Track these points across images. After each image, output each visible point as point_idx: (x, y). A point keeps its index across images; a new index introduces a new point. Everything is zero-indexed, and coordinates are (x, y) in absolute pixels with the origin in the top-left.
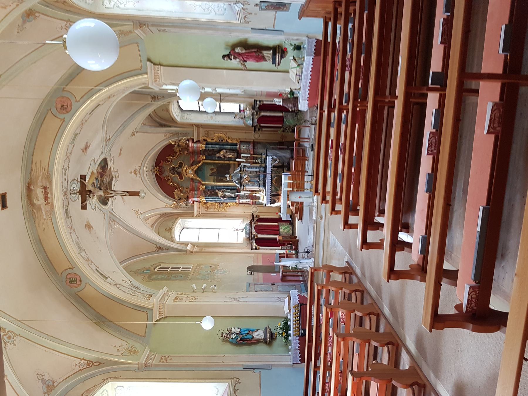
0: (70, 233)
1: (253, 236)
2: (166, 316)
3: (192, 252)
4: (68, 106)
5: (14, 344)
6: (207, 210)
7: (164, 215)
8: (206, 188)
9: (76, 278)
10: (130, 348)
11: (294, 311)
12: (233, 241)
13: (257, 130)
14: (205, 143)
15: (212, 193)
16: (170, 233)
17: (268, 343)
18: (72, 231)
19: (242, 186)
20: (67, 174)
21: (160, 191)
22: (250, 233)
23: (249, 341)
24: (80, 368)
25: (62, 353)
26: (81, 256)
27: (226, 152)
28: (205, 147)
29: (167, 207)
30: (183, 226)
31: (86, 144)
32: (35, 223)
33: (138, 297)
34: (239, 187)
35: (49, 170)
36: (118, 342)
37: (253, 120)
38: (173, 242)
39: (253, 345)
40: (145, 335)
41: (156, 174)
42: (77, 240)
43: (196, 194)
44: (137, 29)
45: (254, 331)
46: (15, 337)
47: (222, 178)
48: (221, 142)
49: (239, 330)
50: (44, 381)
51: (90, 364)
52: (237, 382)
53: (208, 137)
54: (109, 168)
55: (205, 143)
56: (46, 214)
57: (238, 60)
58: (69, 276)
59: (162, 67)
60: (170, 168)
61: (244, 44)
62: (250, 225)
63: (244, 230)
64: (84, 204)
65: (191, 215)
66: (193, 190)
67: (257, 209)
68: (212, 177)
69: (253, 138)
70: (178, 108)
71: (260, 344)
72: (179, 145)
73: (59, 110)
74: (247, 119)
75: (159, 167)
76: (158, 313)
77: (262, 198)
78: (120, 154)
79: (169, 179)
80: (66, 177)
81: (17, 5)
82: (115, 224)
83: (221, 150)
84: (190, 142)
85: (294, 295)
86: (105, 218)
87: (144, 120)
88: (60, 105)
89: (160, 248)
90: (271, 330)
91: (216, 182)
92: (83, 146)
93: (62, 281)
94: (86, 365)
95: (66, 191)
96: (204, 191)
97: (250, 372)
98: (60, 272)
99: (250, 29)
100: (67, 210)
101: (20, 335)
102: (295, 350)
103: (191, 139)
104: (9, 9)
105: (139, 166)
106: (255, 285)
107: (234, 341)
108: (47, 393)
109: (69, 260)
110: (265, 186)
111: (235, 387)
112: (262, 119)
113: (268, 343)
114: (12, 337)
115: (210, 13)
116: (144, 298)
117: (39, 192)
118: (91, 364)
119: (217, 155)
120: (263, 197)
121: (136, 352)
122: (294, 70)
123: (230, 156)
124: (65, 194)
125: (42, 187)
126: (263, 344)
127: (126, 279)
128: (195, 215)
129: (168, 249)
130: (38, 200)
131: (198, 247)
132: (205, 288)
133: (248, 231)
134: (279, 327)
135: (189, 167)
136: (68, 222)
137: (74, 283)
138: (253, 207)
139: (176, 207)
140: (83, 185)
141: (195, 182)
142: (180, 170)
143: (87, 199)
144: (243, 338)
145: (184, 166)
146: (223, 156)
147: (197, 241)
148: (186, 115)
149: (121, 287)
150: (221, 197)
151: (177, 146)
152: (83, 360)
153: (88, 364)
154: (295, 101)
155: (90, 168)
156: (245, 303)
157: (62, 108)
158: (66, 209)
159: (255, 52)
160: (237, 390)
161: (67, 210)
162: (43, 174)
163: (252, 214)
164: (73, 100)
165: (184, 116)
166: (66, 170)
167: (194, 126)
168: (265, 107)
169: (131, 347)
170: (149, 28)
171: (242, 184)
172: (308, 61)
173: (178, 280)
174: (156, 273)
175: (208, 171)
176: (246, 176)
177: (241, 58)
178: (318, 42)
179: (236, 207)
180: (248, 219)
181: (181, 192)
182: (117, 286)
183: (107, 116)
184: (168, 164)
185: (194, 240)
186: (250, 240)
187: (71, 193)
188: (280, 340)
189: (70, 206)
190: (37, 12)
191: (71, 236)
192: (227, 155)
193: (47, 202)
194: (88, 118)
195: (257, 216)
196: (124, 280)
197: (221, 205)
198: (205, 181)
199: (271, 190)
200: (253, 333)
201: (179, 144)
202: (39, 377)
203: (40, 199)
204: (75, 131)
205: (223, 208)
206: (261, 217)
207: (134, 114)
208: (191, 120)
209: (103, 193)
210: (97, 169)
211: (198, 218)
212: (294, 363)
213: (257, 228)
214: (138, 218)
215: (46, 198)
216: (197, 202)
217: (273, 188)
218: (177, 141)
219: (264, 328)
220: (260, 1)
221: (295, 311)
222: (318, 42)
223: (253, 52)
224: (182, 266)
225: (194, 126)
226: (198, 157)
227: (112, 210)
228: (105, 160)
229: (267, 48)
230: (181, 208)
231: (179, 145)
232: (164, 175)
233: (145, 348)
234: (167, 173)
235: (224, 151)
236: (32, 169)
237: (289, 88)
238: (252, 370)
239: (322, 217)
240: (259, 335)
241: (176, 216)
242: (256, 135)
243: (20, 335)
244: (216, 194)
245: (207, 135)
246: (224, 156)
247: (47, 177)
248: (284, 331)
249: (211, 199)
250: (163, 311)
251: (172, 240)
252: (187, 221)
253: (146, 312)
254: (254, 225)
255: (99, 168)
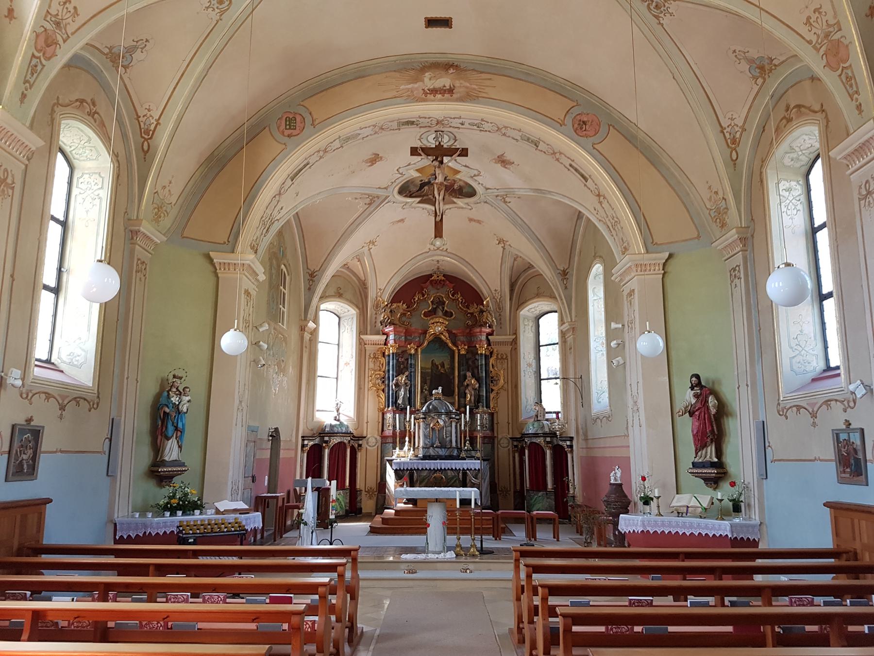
0: (375, 126)
1: (326, 439)
2: (219, 275)
3: (303, 329)
4: (584, 132)
5: (207, 8)
6: (372, 356)
7: (363, 286)
8: (411, 355)
9: (295, 129)
10: (164, 208)
11: (229, 521)
12: (319, 404)
13: (515, 443)
14: (488, 353)
15: (403, 363)
16: (334, 294)
17: (155, 469)
18: (377, 129)
19: (423, 416)
20: (472, 127)
21: (405, 280)
22: (332, 434)
23: (162, 430)
24: (142, 116)
25: (175, 88)
26: (334, 141)
27: (476, 389)
28: (481, 354)
29: (378, 291)
30: (343, 317)
31: (511, 161)
32: (391, 71)
33: (257, 228)
34: (421, 411)
35: (480, 99)
36: (177, 189)
37: (536, 435)
38: (321, 298)
39: (150, 439)
40: (184, 237)
41: (431, 276)
42: (361, 136)
43: (400, 338)
44: (737, 233)
45: (179, 440)
46: (219, 11)
47: (428, 382)
48: (491, 379)
49: (185, 410)
50: (131, 50)
51: (147, 135)
52: (91, 403)
53: (497, 358)
54: (455, 200)
55: (488, 353)
56: (408, 90)
57: (693, 401)
58: (298, 118)
59: (661, 276)
60: (443, 297)
61: (723, 411)
62: (348, 433)
63: (338, 423)
64: (420, 152)
65: (362, 330)
66: (408, 333)
67: (373, 446)
68: (429, 365)
69: (500, 437)
70: (543, 311)
71: (152, 454)
72: (482, 311)
73: (578, 118)
74: (536, 424)
75: (444, 280)
76: (226, 261)
77: (402, 453)
78: (471, 220)
79: (423, 295)
80: (467, 125)
81: (810, 42)
82: (365, 204)
83: (478, 380)
84: (488, 330)
85: (252, 520)
86: (379, 188)
87: (524, 259)
88: (585, 119)
89: (312, 277)
90: (180, 474)
91: (421, 372)
92: (508, 157)
93: (290, 106)
94: (146, 127)
95: (443, 124)
96: (404, 352)
97: (106, 433)
98: (305, 103)
99: (762, 418)
100: (412, 123)
101: (220, 21)
102: (145, 526)
103: (493, 331)
104: (803, 30)
105: (447, 249)
106: (255, 442)
107: (163, 400)
108: (110, 52)
109: (328, 121)
110: (425, 458)
111: (85, 399)
112: (537, 452)
113: (155, 469)
114: (220, 7)
115: (792, 348)
116: (255, 238)
117: (444, 81)
118: (146, 137)
119: (469, 374)
120: (403, 455)
121: (157, 218)
122: (693, 503)
123: (469, 396)
124: (438, 123)
125: (452, 86)
126: (152, 458)
127: (283, 212)
128: (362, 337)
129: (309, 289)
130: (430, 79)
131: (310, 340)
132: (260, 346)
133: (336, 430)
134: (189, 491)
135: (445, 327)
136: (392, 123)
137: (286, 125)
138: (376, 439)
139: (377, 306)
140: (451, 152)
141: (420, 337)
142: (440, 313)
143: (429, 157)
144: (168, 416)
145: (447, 320)
146: (468, 383)
147: (320, 340)
148: (531, 324)
149: (274, 202)
150: (397, 380)
151: (481, 309)
152: (155, 123)
153: (147, 132)
154: (621, 508)
155: (467, 168)
156: (640, 384)
157: (582, 123)
158: (414, 122)
159: (713, 429)
160: (78, 404)
161: (412, 123)
162: (474, 89)
163: (365, 437)
164: (595, 139)
165: (528, 320)
166: (478, 126)
167: (514, 337)
168: (561, 456)
169: (166, 211)
170: (741, 253)
171: (427, 416)
172: (723, 528)
173: (268, 303)
174: (279, 266)
175: (440, 358)
176: (442, 423)
177: (699, 405)
178: (755, 543)
179: (377, 407)
180: (356, 430)
181: (403, 315)
182: (277, 195)
183: (553, 195)
184: (449, 295)
185: (322, 336)
186: (320, 434)
187: (438, 133)
188: (162, 495)
189: (418, 129)
190: (764, 82)
191: (369, 127)
192: (469, 391)
193: (428, 92)
194: (562, 164)
195: (360, 445)
196: (281, 209)
197: (379, 381)
198: (422, 353)
199: (422, 469)
200: (176, 438)
201: (485, 311)
202: (141, 42)
203: (432, 82)
204: (542, 141)
205: (374, 385)
206: (359, 455)
207: (540, 241)
208: (524, 332)
209: (440, 181)
210: (460, 180)
211: (358, 342)
212: (115, 524)
213: (341, 446)
214: (364, 245)
215: (434, 91)
216: (386, 340)
217: (425, 474)
218: (489, 309)
219: (183, 461)
220: (6, 481)
221: (230, 523)
222: (755, 543)
223: (712, 426)
224: (285, 310)
225: (514, 337)
226: (463, 343)
227: (389, 202)
228: (472, 193)
229: (719, 453)
230: (376, 314)
231: (482, 311)
232: (430, 287)
233: (164, 235)
234: (433, 294)
235: (477, 386)
236: (482, 73)
237: (659, 493)
238: (109, 436)
239: (413, 573)
240: (171, 451)
241: (361, 306)
242: (506, 441)
243: (221, 20)
244: (399, 372)
245: (500, 357)
246: (468, 385)
247: (468, 95)
248: (181, 502)
249: (393, 362)
250: (229, 269)
251: (324, 297)
252: (352, 322)
253: (228, 242)
254: (346, 440)
255: (462, 183)
